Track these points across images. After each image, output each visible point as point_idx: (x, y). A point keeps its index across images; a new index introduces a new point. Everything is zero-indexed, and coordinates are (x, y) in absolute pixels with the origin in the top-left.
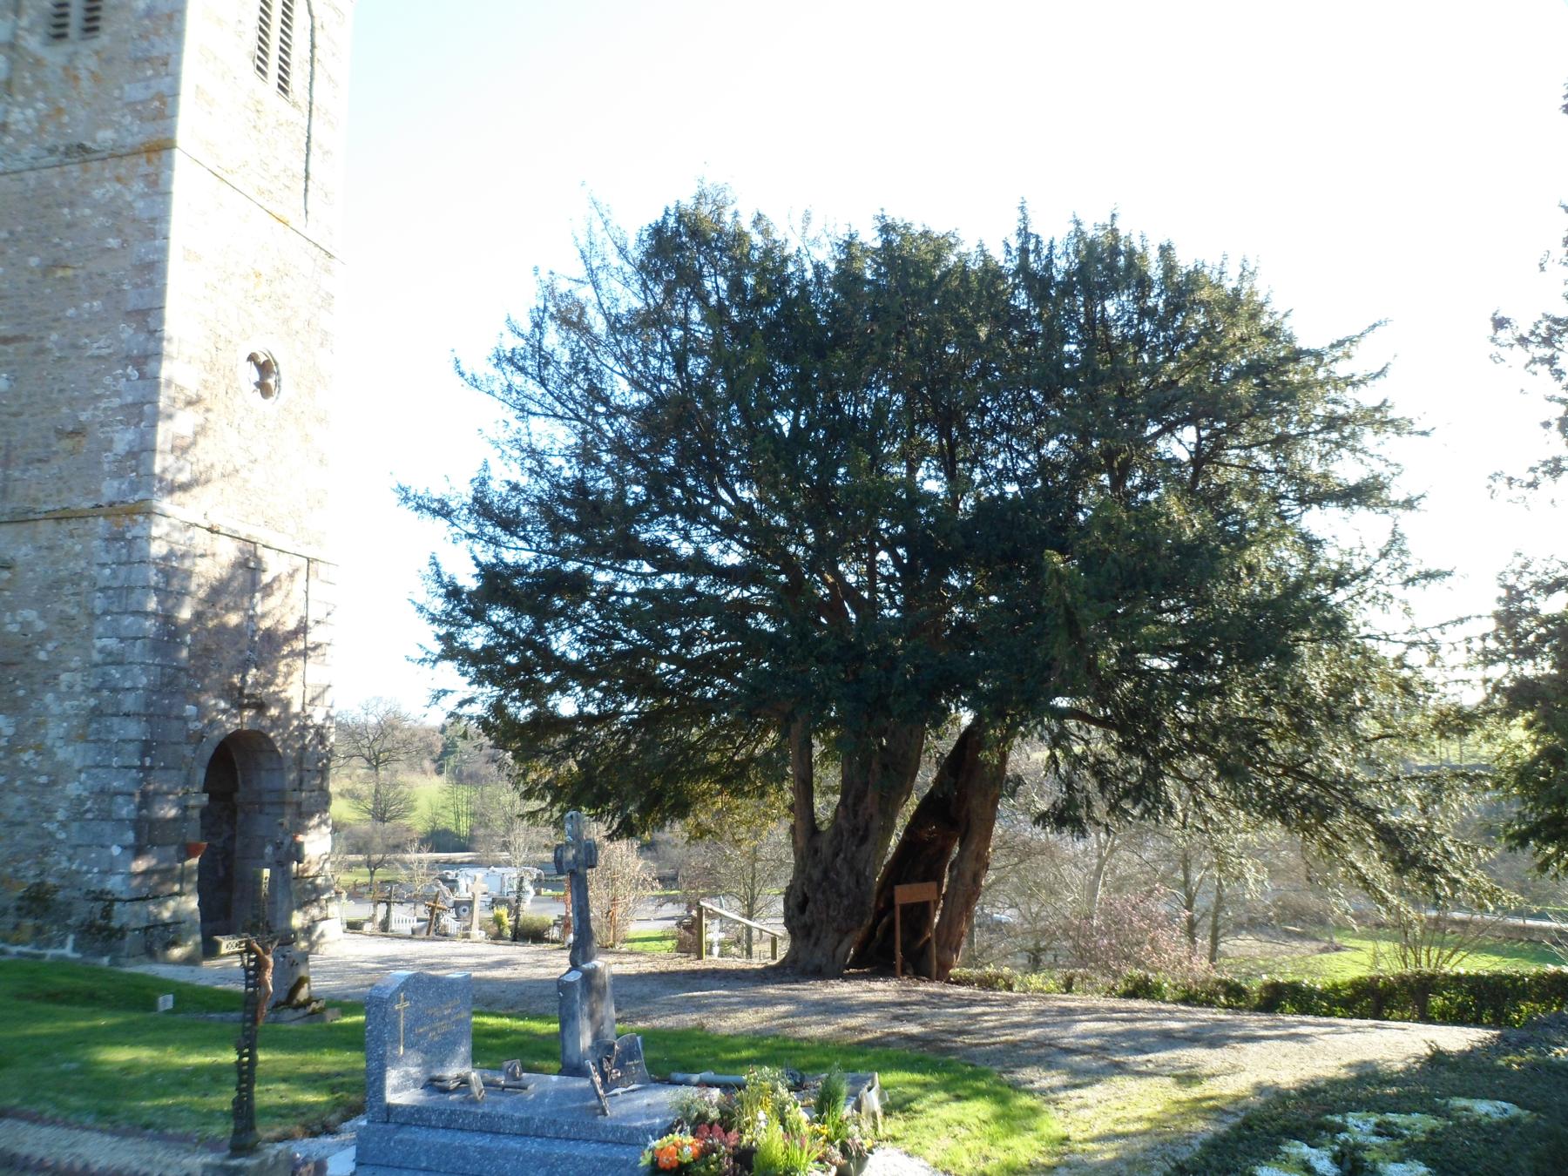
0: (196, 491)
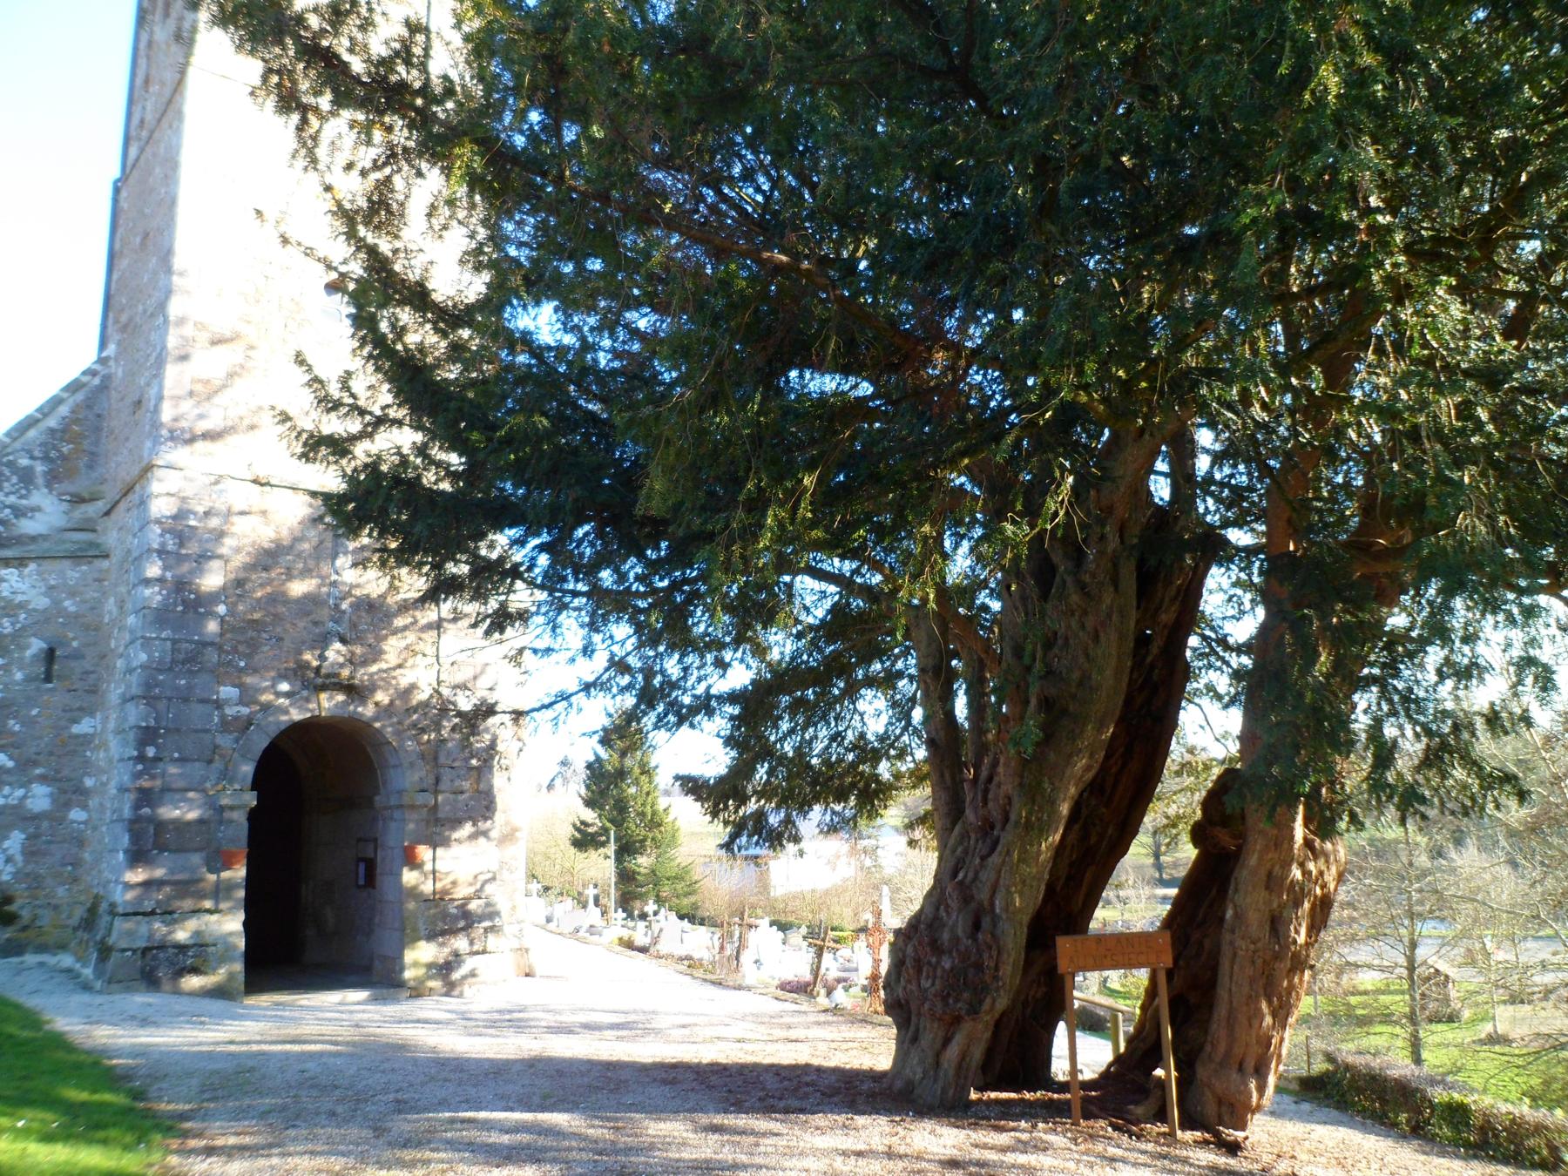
0: (230, 440)
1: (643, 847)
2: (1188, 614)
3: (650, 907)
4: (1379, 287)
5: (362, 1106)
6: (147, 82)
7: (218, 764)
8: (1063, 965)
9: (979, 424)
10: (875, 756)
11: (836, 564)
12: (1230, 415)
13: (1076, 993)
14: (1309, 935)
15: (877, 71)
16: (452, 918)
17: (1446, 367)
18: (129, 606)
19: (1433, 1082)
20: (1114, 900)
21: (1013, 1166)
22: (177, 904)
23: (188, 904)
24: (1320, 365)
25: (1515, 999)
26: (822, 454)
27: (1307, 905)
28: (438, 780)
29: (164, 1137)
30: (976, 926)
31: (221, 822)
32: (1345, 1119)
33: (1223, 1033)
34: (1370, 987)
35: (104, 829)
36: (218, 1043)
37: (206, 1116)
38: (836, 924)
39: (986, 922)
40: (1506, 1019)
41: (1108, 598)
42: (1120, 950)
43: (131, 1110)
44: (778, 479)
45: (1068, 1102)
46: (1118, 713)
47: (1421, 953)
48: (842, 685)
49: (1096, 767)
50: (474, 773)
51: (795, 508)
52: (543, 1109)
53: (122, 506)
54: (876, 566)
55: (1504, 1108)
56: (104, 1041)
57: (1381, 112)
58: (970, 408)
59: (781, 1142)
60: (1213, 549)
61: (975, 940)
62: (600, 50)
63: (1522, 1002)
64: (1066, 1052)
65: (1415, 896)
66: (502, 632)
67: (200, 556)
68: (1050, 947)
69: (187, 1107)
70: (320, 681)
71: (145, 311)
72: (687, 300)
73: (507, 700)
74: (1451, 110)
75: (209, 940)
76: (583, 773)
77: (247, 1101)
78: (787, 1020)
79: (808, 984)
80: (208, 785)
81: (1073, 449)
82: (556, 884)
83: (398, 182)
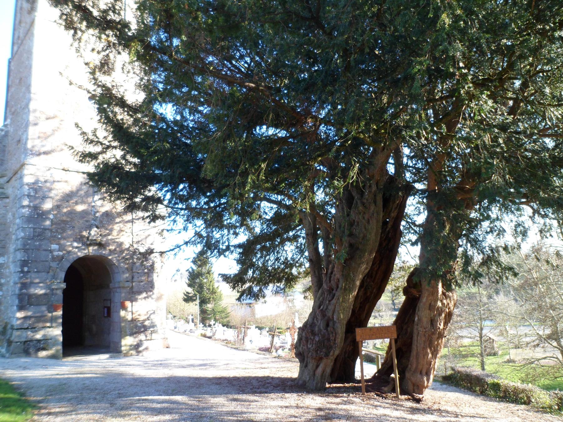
0: (53, 154)
1: (209, 301)
2: (400, 214)
3: (212, 322)
4: (463, 95)
5: (106, 396)
6: (20, 22)
7: (51, 273)
8: (358, 338)
9: (325, 145)
10: (291, 266)
11: (274, 197)
12: (413, 141)
13: (363, 349)
14: (444, 326)
15: (286, 18)
16: (138, 328)
17: (488, 125)
18: (17, 216)
19: (488, 376)
20: (378, 316)
21: (341, 409)
22: (36, 325)
23: (41, 325)
24: (445, 124)
25: (517, 347)
26: (267, 156)
27: (443, 315)
28: (133, 278)
29: (32, 409)
30: (327, 325)
31: (53, 294)
32: (458, 390)
33: (414, 361)
34: (467, 344)
35: (9, 298)
36: (52, 375)
37: (48, 401)
38: (279, 327)
39: (331, 324)
40: (514, 354)
41: (372, 208)
42: (379, 332)
43: (19, 400)
44: (252, 165)
45: (360, 387)
46: (376, 248)
47: (484, 332)
48: (279, 241)
49: (369, 268)
50: (146, 275)
51: (259, 175)
52: (172, 395)
53: (14, 179)
54: (290, 197)
55: (512, 384)
56: (9, 375)
57: (463, 32)
58: (321, 140)
59: (258, 404)
60: (409, 190)
61: (327, 330)
62: (184, 8)
63: (519, 348)
64: (360, 370)
65: (482, 312)
66: (154, 222)
67: (43, 197)
68: (353, 332)
69: (41, 398)
70: (88, 243)
71: (21, 107)
72: (218, 100)
73: (158, 248)
74: (487, 32)
75: (49, 337)
76: (186, 274)
77: (63, 396)
78: (261, 361)
79: (269, 348)
80: (48, 281)
81: (359, 154)
82: (178, 315)
83: (111, 56)
